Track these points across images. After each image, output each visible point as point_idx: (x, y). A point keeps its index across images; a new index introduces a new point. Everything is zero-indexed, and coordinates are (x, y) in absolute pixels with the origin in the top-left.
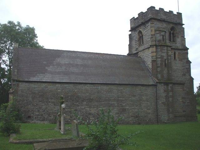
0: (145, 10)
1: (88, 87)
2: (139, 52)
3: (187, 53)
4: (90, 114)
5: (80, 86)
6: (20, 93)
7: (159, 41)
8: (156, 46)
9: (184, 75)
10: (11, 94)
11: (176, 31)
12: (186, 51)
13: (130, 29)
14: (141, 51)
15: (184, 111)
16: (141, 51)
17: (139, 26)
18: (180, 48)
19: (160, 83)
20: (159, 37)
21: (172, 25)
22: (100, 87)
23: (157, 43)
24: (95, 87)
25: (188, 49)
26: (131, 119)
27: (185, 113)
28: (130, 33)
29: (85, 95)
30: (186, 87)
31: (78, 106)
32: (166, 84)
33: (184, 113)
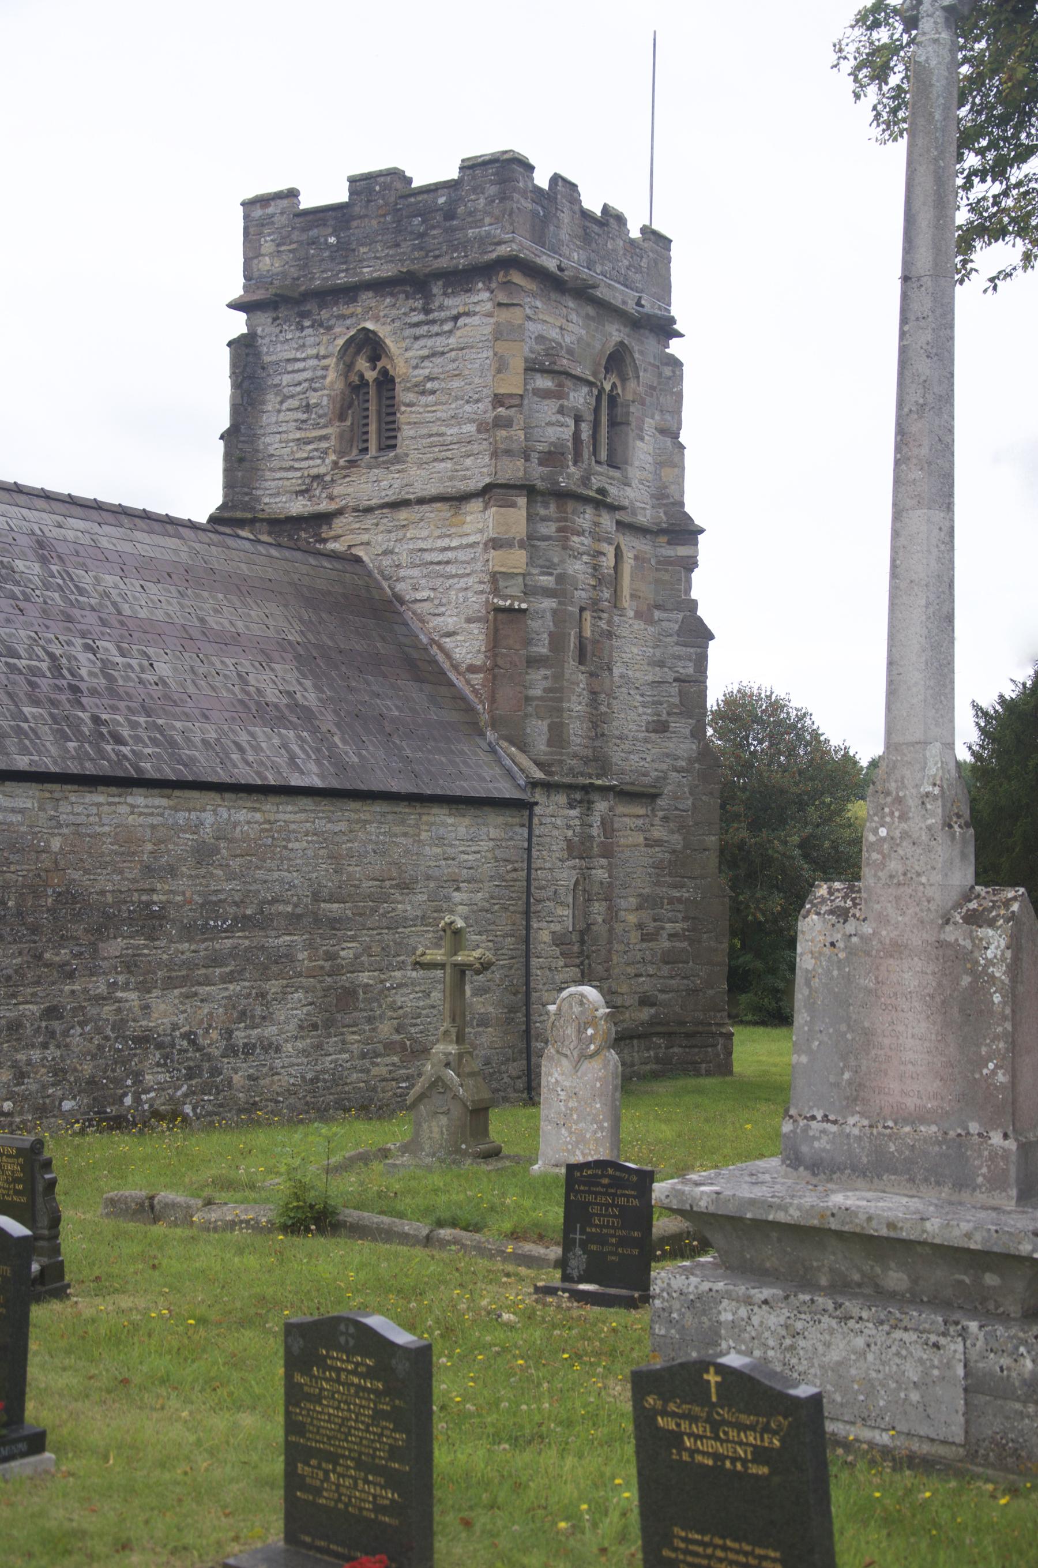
2: (340, 512)
3: (690, 564)
4: (143, 1040)
7: (552, 457)
8: (530, 491)
9: (660, 727)
12: (682, 551)
13: (236, 289)
14: (369, 510)
15: (645, 1001)
16: (369, 510)
18: (645, 517)
19: (548, 787)
20: (553, 427)
22: (208, 818)
24: (181, 817)
25: (702, 531)
26: (383, 1071)
27: (653, 1011)
28: (238, 324)
29: (117, 878)
30: (665, 819)
31: (71, 976)
32: (582, 794)
33: (645, 1014)
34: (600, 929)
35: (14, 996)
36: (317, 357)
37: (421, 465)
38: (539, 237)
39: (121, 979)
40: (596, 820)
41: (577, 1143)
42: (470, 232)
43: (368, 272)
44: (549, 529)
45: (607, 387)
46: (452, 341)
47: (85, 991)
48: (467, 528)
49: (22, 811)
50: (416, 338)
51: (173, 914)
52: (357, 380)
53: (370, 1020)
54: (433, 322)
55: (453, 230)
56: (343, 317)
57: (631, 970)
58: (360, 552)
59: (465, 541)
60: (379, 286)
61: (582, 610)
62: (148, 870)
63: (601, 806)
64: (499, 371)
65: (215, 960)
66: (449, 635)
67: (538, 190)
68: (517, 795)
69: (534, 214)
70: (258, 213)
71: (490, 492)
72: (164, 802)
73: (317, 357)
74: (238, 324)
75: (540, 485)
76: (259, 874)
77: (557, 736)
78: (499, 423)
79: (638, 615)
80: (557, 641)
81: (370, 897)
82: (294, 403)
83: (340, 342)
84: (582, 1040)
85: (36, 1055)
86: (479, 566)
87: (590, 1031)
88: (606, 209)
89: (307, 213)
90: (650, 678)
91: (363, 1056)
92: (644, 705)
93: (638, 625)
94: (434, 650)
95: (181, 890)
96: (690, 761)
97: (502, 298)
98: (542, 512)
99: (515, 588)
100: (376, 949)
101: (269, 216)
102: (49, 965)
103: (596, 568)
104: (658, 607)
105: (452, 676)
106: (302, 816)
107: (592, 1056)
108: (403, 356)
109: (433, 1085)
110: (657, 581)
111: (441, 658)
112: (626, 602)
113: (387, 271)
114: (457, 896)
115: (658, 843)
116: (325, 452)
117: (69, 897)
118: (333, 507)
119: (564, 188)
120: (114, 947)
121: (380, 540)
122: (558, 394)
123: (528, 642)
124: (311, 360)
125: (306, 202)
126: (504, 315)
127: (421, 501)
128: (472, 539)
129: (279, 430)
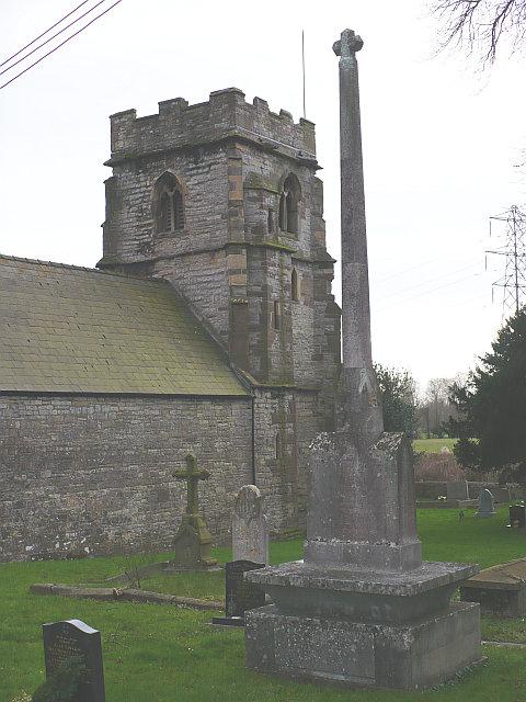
0: (197, 95)
1: (55, 409)
4: (64, 517)
5: (30, 406)
12: (326, 271)
13: (108, 157)
17: (170, 154)
18: (307, 254)
22: (91, 410)
23: (251, 235)
28: (108, 172)
32: (278, 392)
54: (199, 168)
60: (170, 154)
85: (12, 524)
102: (17, 482)
124: (143, 187)
125: (139, 115)
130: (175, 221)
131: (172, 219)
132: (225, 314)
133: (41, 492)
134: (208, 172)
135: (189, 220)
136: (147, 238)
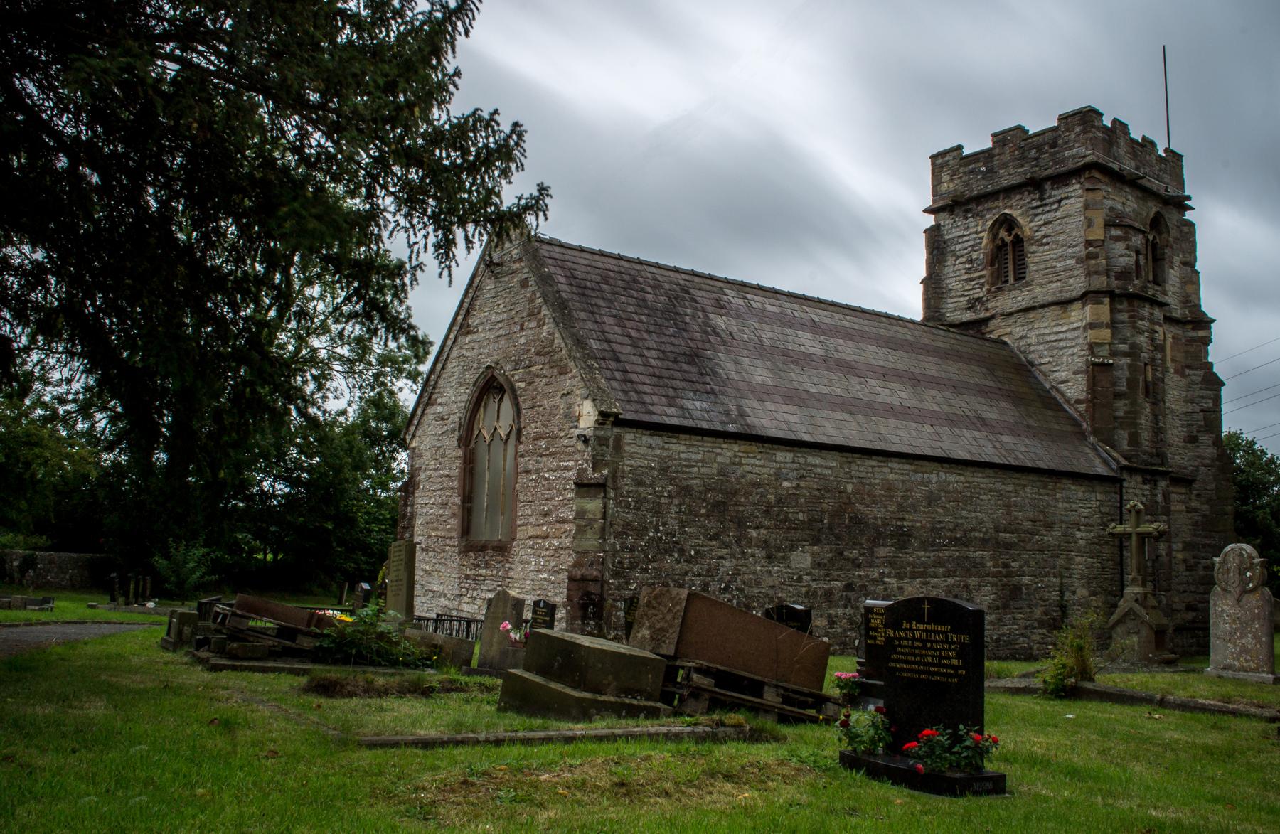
1: (893, 472)
2: (993, 317)
3: (1207, 341)
5: (863, 467)
6: (627, 484)
7: (1124, 275)
10: (592, 491)
11: (1165, 236)
12: (1201, 333)
13: (929, 202)
16: (1010, 314)
18: (1177, 313)
19: (1131, 470)
20: (1122, 256)
21: (1153, 208)
22: (934, 478)
24: (919, 477)
28: (930, 220)
30: (1198, 495)
31: (859, 566)
32: (1151, 475)
34: (1164, 559)
35: (828, 575)
36: (977, 233)
37: (1041, 285)
38: (1108, 153)
39: (887, 570)
40: (1159, 492)
41: (1241, 652)
42: (1066, 154)
43: (1006, 182)
44: (1124, 317)
45: (1151, 238)
46: (1058, 214)
47: (867, 576)
48: (1073, 319)
49: (831, 468)
50: (1036, 215)
51: (915, 533)
52: (999, 243)
53: (1029, 606)
54: (1046, 205)
55: (1056, 153)
56: (990, 209)
57: (1181, 588)
58: (1006, 339)
59: (1071, 327)
60: (1009, 191)
61: (1146, 364)
62: (901, 507)
63: (1163, 484)
64: (1089, 227)
65: (939, 563)
66: (1063, 382)
67: (1105, 126)
68: (1112, 474)
69: (1104, 139)
70: (939, 161)
71: (1085, 297)
72: (908, 467)
73: (977, 233)
74: (930, 220)
75: (1118, 291)
76: (964, 513)
77: (1134, 440)
78: (1090, 256)
79: (1176, 372)
80: (1132, 383)
81: (1028, 531)
82: (964, 259)
83: (990, 223)
84: (1244, 582)
85: (840, 611)
86: (1080, 341)
87: (1249, 574)
88: (1144, 137)
89: (968, 156)
90: (1184, 410)
91: (1026, 628)
92: (1182, 426)
93: (1177, 378)
94: (1054, 393)
95: (917, 520)
96: (1213, 460)
97: (1088, 186)
98: (1119, 307)
99: (1105, 351)
100: (1032, 563)
101: (944, 162)
102: (847, 559)
103: (1153, 340)
104: (1189, 367)
105: (1066, 406)
106: (986, 480)
107: (1252, 591)
108: (1028, 226)
109: (1126, 615)
110: (1186, 352)
111: (1058, 396)
112: (1169, 364)
113: (1017, 180)
114: (1079, 534)
115: (1195, 510)
116: (983, 284)
117: (857, 521)
118: (988, 314)
119: (1120, 128)
120: (882, 552)
121: (1018, 331)
122: (1126, 239)
123: (1114, 384)
124: (973, 234)
125: (966, 152)
126: (1091, 195)
127: (1043, 306)
128: (1075, 325)
129: (955, 274)
130: (1014, 264)
131: (1011, 268)
132: (1081, 381)
133: (875, 574)
134: (1057, 210)
135: (1032, 268)
136: (979, 293)
